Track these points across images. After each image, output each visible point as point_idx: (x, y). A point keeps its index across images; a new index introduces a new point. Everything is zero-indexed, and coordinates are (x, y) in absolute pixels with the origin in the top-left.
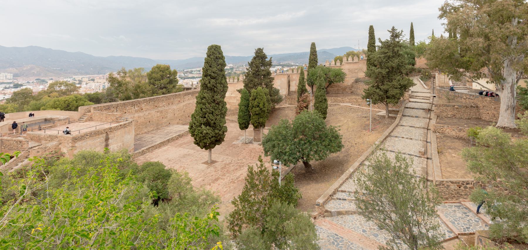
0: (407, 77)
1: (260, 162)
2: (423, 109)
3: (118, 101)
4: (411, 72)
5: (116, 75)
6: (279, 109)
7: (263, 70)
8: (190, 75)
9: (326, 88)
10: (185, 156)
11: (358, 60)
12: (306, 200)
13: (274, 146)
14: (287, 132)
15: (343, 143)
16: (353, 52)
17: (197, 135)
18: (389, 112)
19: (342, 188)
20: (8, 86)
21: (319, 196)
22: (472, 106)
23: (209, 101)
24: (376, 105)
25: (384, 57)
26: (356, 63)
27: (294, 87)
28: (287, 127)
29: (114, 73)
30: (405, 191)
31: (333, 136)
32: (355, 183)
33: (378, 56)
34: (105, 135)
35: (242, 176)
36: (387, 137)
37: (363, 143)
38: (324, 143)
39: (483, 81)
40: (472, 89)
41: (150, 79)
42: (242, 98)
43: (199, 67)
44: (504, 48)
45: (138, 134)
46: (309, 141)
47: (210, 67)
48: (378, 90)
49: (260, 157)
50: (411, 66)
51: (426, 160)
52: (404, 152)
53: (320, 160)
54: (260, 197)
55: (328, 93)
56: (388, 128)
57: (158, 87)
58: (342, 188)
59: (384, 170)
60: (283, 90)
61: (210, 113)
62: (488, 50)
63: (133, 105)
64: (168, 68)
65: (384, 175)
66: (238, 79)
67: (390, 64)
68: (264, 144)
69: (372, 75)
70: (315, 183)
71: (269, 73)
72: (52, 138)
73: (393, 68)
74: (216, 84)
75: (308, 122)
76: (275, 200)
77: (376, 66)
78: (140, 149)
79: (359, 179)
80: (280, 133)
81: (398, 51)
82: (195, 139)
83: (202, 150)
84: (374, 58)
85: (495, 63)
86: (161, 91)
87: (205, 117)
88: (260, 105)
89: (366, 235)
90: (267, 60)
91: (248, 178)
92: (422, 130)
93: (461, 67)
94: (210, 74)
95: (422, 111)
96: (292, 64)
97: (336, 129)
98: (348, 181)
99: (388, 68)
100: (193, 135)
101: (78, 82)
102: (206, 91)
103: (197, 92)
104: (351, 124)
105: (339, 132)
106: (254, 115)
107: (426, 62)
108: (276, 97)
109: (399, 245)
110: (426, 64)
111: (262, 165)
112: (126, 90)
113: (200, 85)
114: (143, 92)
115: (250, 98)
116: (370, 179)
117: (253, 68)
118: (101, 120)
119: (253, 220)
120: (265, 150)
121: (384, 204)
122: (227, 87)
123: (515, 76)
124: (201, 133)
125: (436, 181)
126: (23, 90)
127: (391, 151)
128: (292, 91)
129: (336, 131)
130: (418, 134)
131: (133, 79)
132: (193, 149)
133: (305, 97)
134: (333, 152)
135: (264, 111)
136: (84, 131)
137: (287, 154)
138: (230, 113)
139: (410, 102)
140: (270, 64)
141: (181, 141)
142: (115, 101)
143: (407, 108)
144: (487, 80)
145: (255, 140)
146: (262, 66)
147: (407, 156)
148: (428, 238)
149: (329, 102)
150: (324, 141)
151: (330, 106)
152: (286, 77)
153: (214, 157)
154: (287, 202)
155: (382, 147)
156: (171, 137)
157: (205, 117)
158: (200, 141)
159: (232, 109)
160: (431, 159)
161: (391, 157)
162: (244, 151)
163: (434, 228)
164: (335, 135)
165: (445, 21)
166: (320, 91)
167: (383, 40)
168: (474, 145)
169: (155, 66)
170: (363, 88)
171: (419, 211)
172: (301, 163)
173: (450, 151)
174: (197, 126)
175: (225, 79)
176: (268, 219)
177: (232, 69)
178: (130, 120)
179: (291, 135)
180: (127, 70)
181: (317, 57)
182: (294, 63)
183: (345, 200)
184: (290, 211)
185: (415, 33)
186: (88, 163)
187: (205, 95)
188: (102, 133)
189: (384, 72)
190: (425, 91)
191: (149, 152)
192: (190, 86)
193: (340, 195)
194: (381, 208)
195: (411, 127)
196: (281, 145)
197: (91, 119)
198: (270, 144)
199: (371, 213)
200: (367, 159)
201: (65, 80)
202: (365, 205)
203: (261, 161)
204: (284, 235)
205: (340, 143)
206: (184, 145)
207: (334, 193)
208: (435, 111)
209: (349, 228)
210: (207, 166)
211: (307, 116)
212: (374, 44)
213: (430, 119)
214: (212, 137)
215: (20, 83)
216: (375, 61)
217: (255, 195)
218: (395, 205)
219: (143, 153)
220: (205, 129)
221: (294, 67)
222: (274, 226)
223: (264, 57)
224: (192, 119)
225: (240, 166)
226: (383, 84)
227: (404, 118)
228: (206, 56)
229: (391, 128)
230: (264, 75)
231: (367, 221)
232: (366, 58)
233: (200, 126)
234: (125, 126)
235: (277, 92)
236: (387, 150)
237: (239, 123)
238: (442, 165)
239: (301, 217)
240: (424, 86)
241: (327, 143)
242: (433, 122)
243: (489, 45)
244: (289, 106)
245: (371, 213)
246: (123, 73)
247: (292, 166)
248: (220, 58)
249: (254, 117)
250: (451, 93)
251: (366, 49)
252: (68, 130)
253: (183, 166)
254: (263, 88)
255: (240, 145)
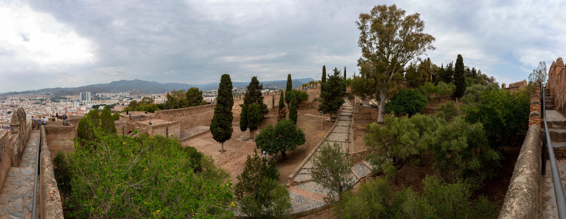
0: (341, 98)
1: (255, 152)
2: (348, 116)
3: (171, 109)
4: (343, 95)
5: (170, 94)
6: (267, 118)
7: (257, 92)
8: (210, 95)
9: (297, 104)
10: (207, 145)
11: (316, 87)
12: (283, 176)
13: (263, 143)
14: (271, 133)
15: (306, 139)
16: (313, 81)
17: (214, 133)
18: (332, 118)
19: (305, 167)
20: (128, 99)
21: (290, 173)
22: (369, 113)
23: (222, 112)
24: (325, 115)
25: (331, 86)
26: (315, 88)
27: (277, 104)
28: (272, 129)
29: (169, 93)
30: (338, 163)
31: (300, 135)
32: (311, 162)
33: (327, 85)
34: (166, 127)
35: (242, 161)
36: (330, 133)
37: (317, 138)
38: (294, 140)
39: (373, 100)
40: (369, 104)
41: (187, 97)
42: (242, 110)
43: (215, 89)
44: (381, 84)
45: (182, 129)
46: (285, 139)
47: (223, 89)
48: (326, 106)
49: (255, 149)
50: (343, 92)
51: (348, 143)
52: (338, 141)
53: (292, 150)
54: (255, 175)
55: (298, 107)
56: (331, 128)
57: (192, 101)
58: (305, 167)
59: (328, 153)
60: (270, 105)
61: (222, 120)
62: (376, 84)
63: (179, 111)
64: (197, 90)
65: (328, 156)
66: (240, 98)
67: (334, 90)
68: (256, 141)
69: (324, 96)
70: (288, 165)
71: (261, 94)
72: (145, 125)
73: (335, 92)
74: (226, 100)
75: (285, 126)
76: (264, 177)
77: (326, 91)
78: (183, 138)
79: (314, 160)
80: (267, 134)
81: (338, 82)
82: (214, 135)
83: (217, 142)
84: (325, 85)
85: (378, 92)
86: (193, 104)
87: (219, 122)
88: (254, 115)
89: (317, 193)
90: (260, 85)
91: (247, 163)
92: (347, 127)
93: (365, 93)
94: (223, 93)
95: (348, 117)
96: (276, 88)
97: (302, 130)
98: (308, 162)
99: (332, 92)
100: (212, 133)
101: (153, 98)
102: (220, 105)
103: (214, 105)
104: (310, 127)
105: (304, 132)
106: (250, 122)
107: (351, 89)
108: (265, 110)
109: (333, 194)
110: (350, 91)
111: (256, 155)
112: (176, 103)
113: (216, 101)
114: (184, 104)
115: (248, 111)
116: (320, 159)
117: (250, 90)
118: (164, 119)
119: (250, 190)
120: (257, 145)
121: (327, 172)
122: (234, 103)
123: (384, 98)
124: (217, 132)
125: (352, 154)
126: (133, 101)
127: (332, 141)
128: (275, 106)
129: (302, 132)
130: (345, 129)
131: (179, 96)
132: (212, 141)
133: (283, 110)
134: (300, 145)
135: (257, 119)
136: (157, 124)
137: (271, 147)
138: (234, 120)
139: (343, 112)
140: (261, 88)
141: (205, 136)
142: (170, 109)
143: (341, 115)
144: (375, 100)
145: (251, 138)
146: (256, 89)
147: (339, 143)
148: (347, 185)
149: (298, 114)
150: (294, 138)
151: (299, 116)
152: (272, 96)
153: (225, 148)
154: (272, 178)
155: (327, 139)
156: (199, 133)
157: (219, 122)
158: (217, 137)
159: (236, 117)
160: (350, 143)
161: (332, 144)
162: (244, 145)
163: (350, 180)
164: (301, 134)
165: (360, 68)
166: (293, 106)
167: (330, 75)
168: (368, 132)
169: (190, 88)
170: (318, 104)
171: (344, 172)
172: (280, 153)
173: (359, 137)
174: (215, 127)
175: (232, 97)
176: (260, 189)
177: (236, 90)
178: (178, 120)
179: (274, 135)
180: (176, 91)
181: (291, 84)
182: (277, 87)
183: (306, 174)
184: (273, 184)
185: (346, 73)
186: (160, 141)
187: (220, 107)
188: (165, 126)
189: (330, 94)
190: (350, 105)
191: (188, 140)
192: (210, 102)
193: (303, 171)
194: (325, 175)
195: (342, 126)
196: (267, 142)
197: (159, 118)
198: (260, 141)
199: (320, 179)
200: (319, 147)
201: (148, 96)
202: (317, 175)
203: (256, 152)
204: (269, 199)
205: (304, 139)
206: (207, 139)
207: (300, 170)
208: (354, 116)
209: (307, 190)
210: (221, 153)
211: (284, 122)
212: (326, 77)
213: (351, 121)
214: (224, 135)
215: (132, 97)
216: (326, 87)
217: (251, 174)
218: (332, 172)
219: (184, 140)
220: (220, 130)
221: (277, 90)
222: (264, 194)
223: (257, 83)
224: (212, 123)
225: (241, 154)
226: (329, 102)
227: (340, 122)
228: (220, 82)
229: (332, 128)
230: (257, 95)
231: (318, 184)
232: (321, 86)
233: (216, 127)
234: (175, 124)
235: (266, 106)
236: (330, 141)
237: (241, 127)
238: (355, 145)
239: (280, 187)
240: (350, 103)
241: (296, 139)
242: (353, 122)
243: (376, 83)
244: (273, 116)
245: (320, 179)
246: (174, 92)
247: (274, 155)
248: (229, 83)
249: (250, 123)
250: (361, 107)
251: (321, 80)
252: (151, 122)
253: (206, 151)
254: (256, 104)
255: (241, 141)
